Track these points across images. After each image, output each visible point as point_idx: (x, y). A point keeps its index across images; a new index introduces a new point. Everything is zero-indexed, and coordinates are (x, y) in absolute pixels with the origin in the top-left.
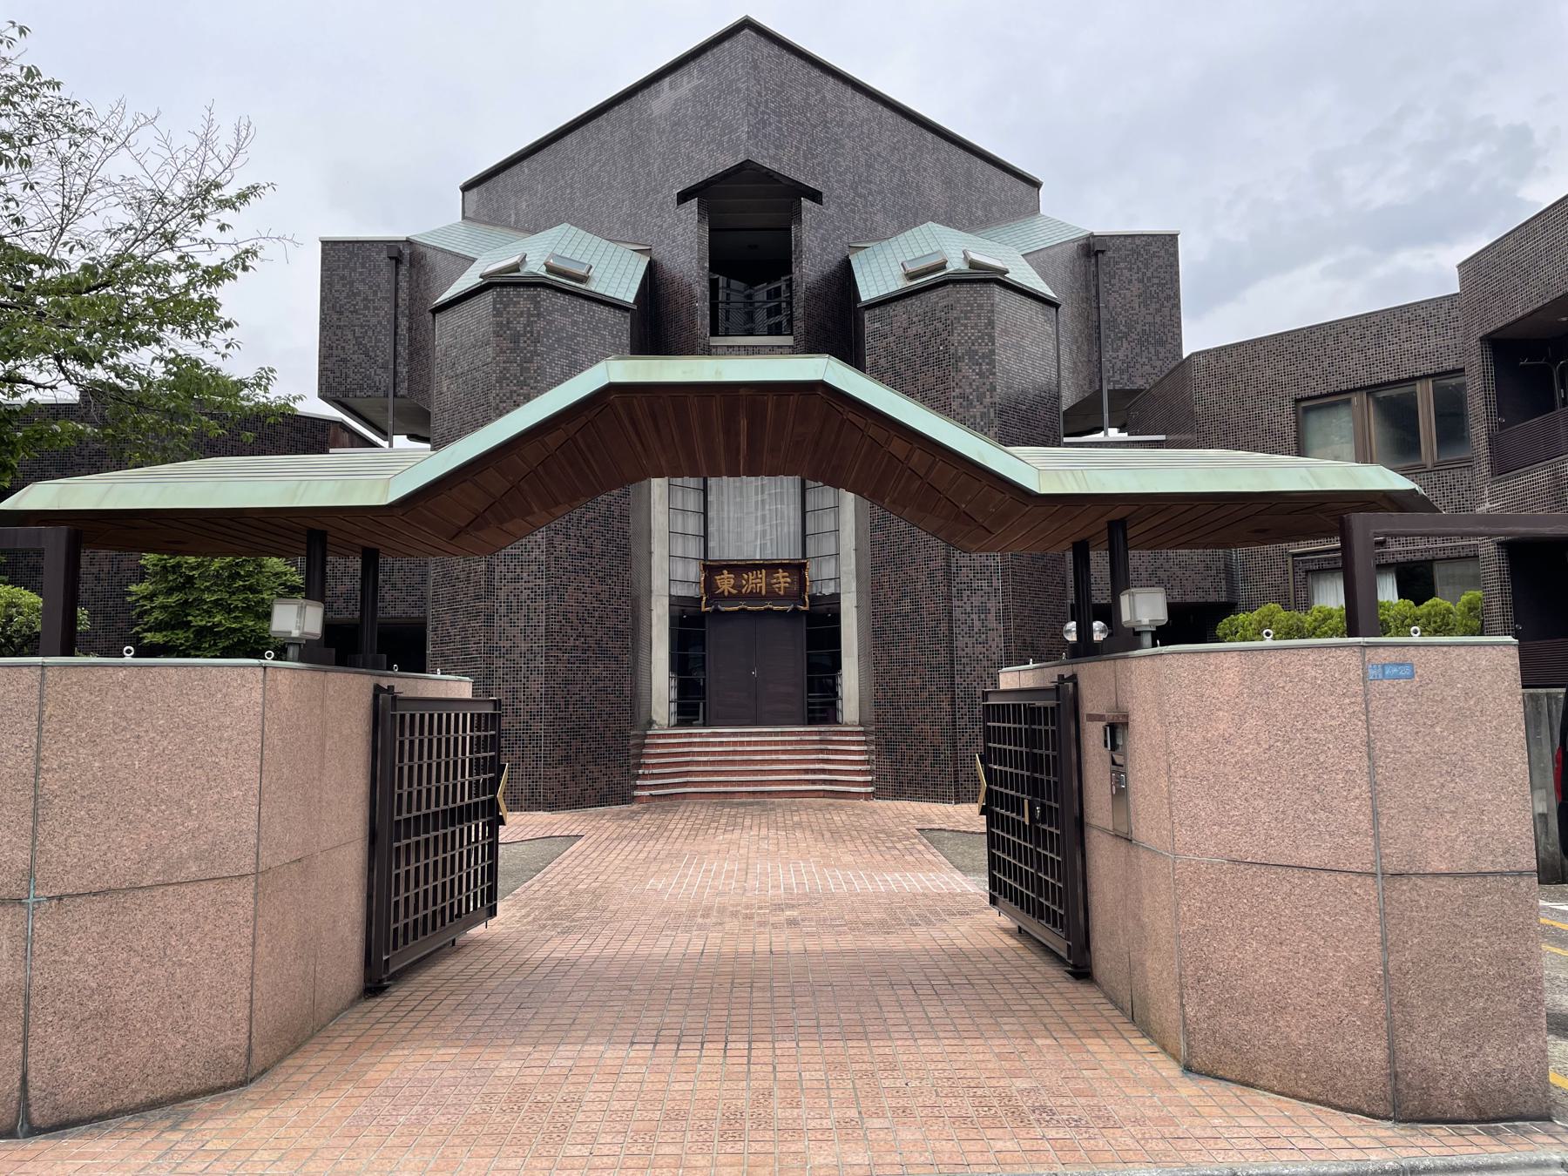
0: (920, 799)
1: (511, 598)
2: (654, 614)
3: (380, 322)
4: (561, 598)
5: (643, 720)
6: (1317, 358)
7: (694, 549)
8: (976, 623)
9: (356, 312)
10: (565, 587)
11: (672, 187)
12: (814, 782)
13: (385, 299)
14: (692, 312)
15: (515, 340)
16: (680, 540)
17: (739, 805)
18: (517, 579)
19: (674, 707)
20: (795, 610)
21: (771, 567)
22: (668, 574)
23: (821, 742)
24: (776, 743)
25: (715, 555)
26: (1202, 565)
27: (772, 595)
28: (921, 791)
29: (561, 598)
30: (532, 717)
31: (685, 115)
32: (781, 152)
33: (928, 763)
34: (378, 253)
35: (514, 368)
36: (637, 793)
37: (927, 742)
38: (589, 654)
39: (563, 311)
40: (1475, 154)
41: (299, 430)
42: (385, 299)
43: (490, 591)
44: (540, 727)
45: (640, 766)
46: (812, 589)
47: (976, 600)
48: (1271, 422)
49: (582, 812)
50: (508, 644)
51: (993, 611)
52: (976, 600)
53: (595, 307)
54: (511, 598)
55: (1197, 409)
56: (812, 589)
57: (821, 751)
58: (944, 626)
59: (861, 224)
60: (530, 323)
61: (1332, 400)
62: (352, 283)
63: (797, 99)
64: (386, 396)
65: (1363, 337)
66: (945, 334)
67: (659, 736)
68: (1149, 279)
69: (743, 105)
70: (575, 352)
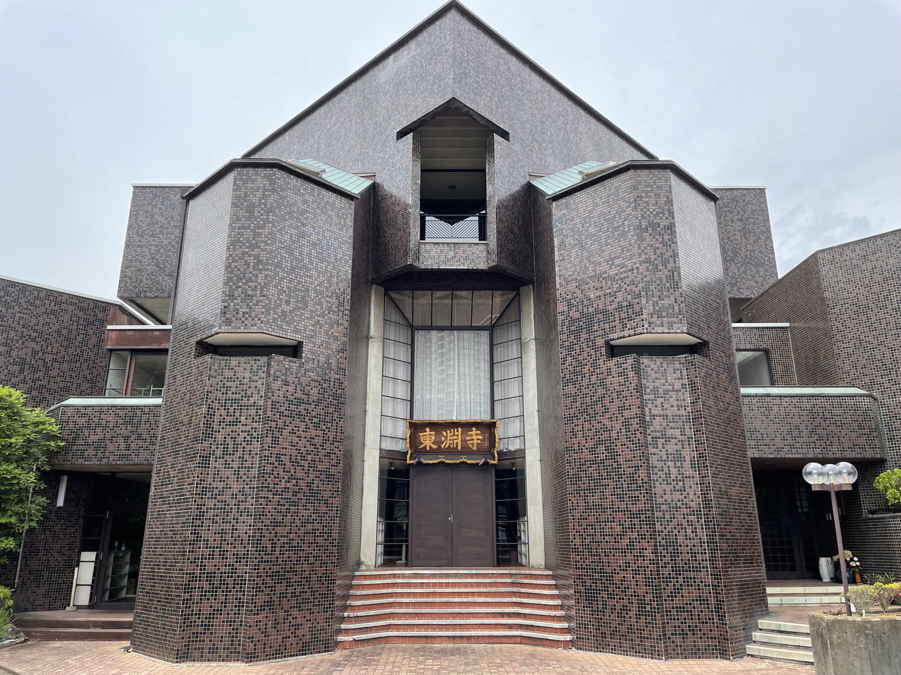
0: (625, 653)
1: (228, 440)
2: (366, 465)
3: (170, 243)
4: (275, 441)
5: (352, 561)
7: (402, 411)
8: (673, 470)
9: (153, 235)
10: (280, 430)
11: (393, 129)
12: (510, 627)
13: (176, 227)
14: (406, 217)
15: (250, 210)
16: (391, 404)
17: (444, 652)
19: (381, 549)
20: (486, 463)
21: (467, 426)
22: (379, 433)
23: (513, 584)
24: (472, 585)
25: (418, 417)
26: (855, 425)
27: (466, 451)
28: (626, 645)
29: (275, 441)
30: (238, 559)
31: (405, 77)
32: (478, 98)
33: (632, 614)
34: (175, 196)
35: (248, 233)
36: (340, 638)
37: (630, 592)
38: (300, 496)
39: (296, 191)
41: (81, 309)
42: (176, 227)
43: (209, 433)
44: (245, 570)
45: (345, 608)
46: (500, 446)
47: (671, 448)
49: (281, 662)
50: (221, 485)
51: (688, 458)
53: (324, 191)
54: (228, 440)
55: (827, 294)
56: (500, 446)
57: (514, 594)
58: (642, 473)
59: (537, 161)
60: (264, 197)
62: (152, 216)
63: (490, 64)
64: (169, 297)
67: (366, 577)
68: (747, 220)
69: (450, 60)
70: (303, 225)
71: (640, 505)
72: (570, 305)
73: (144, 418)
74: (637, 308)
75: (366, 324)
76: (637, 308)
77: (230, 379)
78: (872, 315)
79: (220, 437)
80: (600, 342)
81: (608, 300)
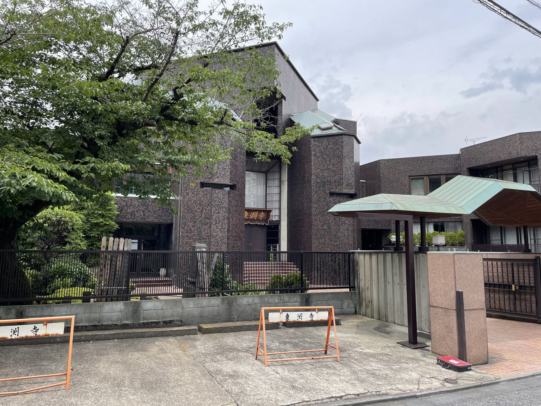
6: (416, 166)
18: (219, 213)
21: (259, 211)
40: (335, 91)
48: (402, 181)
50: (215, 234)
52: (346, 227)
61: (419, 177)
65: (428, 162)
66: (341, 149)
71: (338, 243)
72: (317, 177)
73: (150, 204)
74: (341, 183)
75: (378, 217)
76: (341, 183)
77: (216, 197)
78: (394, 184)
79: (214, 218)
80: (328, 192)
81: (332, 178)
